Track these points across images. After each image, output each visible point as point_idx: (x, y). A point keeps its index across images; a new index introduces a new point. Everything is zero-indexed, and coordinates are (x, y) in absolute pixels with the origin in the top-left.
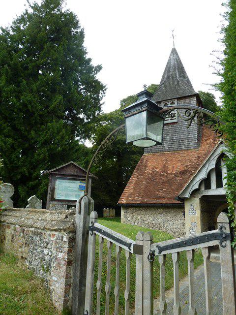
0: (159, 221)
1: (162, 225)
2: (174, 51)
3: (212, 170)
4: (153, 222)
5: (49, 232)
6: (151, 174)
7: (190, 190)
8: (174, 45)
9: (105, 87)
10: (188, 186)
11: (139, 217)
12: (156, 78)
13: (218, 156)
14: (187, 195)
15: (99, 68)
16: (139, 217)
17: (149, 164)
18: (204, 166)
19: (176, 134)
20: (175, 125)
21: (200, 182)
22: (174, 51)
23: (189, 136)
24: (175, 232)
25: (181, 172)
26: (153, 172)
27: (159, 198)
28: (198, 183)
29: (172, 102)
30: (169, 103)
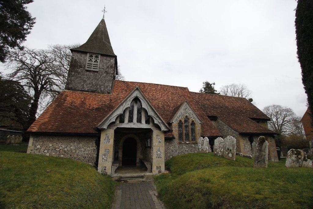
0: (72, 148)
1: (74, 151)
2: (103, 22)
3: (126, 109)
4: (66, 149)
6: (70, 108)
7: (108, 123)
9: (32, 20)
10: (107, 119)
11: (51, 145)
12: (82, 39)
13: (133, 98)
14: (105, 127)
16: (51, 145)
18: (122, 104)
19: (96, 81)
20: (96, 73)
21: (116, 116)
22: (103, 22)
23: (105, 84)
24: (85, 157)
25: (96, 109)
26: (72, 105)
27: (75, 128)
28: (115, 118)
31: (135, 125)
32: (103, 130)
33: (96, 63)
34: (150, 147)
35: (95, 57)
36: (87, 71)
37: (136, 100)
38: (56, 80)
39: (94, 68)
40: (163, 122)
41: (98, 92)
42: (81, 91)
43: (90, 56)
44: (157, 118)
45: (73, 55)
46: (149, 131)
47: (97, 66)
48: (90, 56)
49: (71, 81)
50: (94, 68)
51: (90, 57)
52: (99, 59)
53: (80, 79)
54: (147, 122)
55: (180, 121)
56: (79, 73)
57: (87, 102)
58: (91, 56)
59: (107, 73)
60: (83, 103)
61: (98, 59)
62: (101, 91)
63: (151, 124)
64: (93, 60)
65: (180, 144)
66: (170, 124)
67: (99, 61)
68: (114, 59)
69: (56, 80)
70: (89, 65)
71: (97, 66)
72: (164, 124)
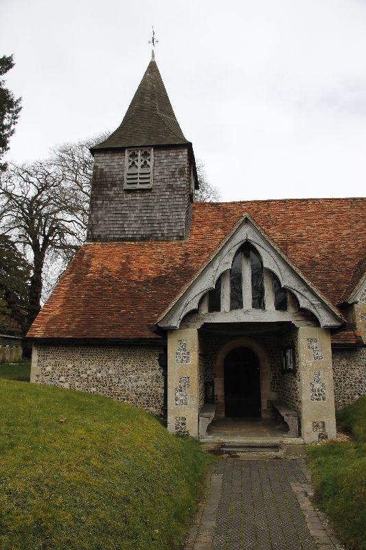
2: (153, 68)
8: (153, 56)
14: (175, 323)
22: (153, 68)
29: (146, 153)
31: (248, 314)
34: (294, 372)
35: (142, 155)
36: (128, 191)
38: (69, 222)
40: (323, 303)
41: (157, 239)
42: (119, 240)
44: (307, 294)
46: (287, 331)
47: (147, 176)
48: (131, 156)
49: (98, 221)
51: (131, 159)
57: (134, 266)
58: (134, 155)
60: (125, 269)
61: (149, 160)
62: (163, 235)
63: (291, 310)
64: (139, 164)
67: (150, 163)
68: (185, 152)
70: (130, 177)
71: (147, 176)
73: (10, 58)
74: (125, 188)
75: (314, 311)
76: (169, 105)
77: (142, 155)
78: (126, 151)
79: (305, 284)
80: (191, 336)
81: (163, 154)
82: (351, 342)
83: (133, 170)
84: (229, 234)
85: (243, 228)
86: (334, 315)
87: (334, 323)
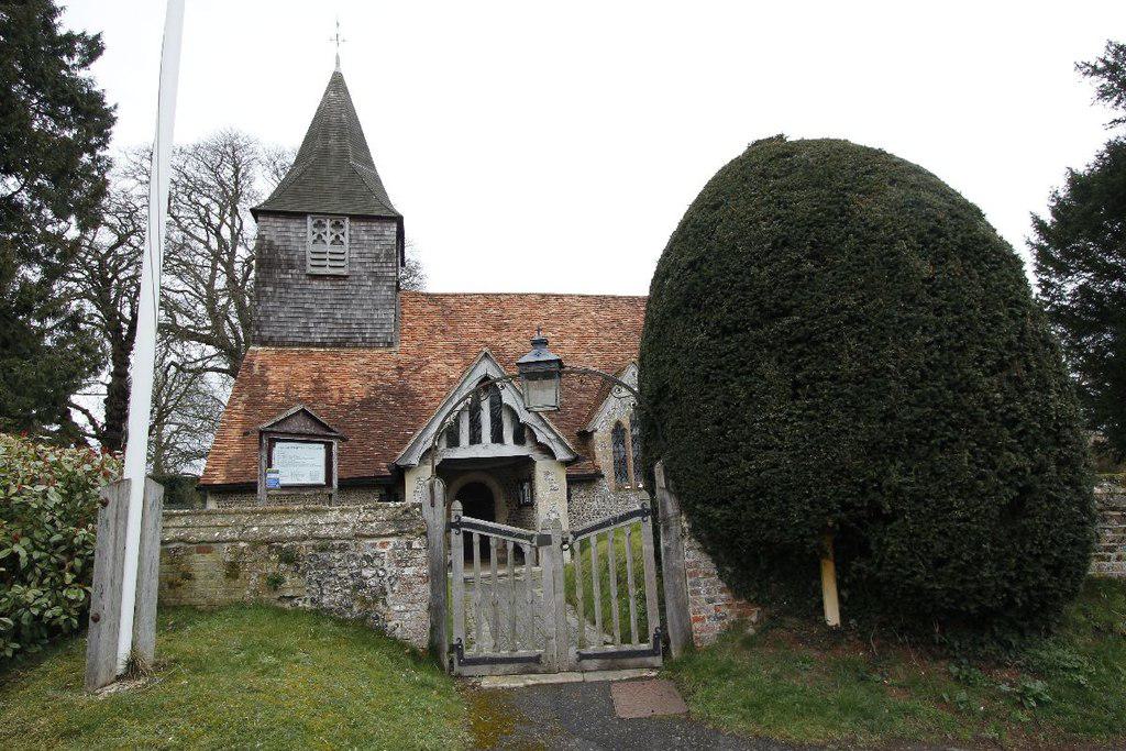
2: (337, 83)
5: (370, 541)
8: (338, 64)
10: (417, 441)
14: (415, 460)
15: (94, 48)
17: (272, 376)
22: (337, 83)
29: (337, 223)
30: (328, 223)
31: (487, 450)
32: (409, 468)
33: (337, 249)
34: (531, 505)
35: (333, 226)
37: (487, 384)
38: (177, 292)
39: (333, 264)
40: (558, 438)
41: (356, 346)
42: (301, 344)
43: (315, 226)
44: (543, 429)
45: (262, 229)
46: (526, 463)
47: (341, 257)
48: (315, 226)
49: (268, 317)
50: (333, 264)
51: (316, 230)
52: (347, 234)
53: (293, 305)
54: (519, 439)
55: (618, 424)
56: (287, 286)
57: (333, 382)
58: (319, 225)
59: (377, 278)
60: (319, 387)
61: (343, 234)
62: (364, 339)
63: (529, 444)
64: (329, 239)
65: (620, 490)
66: (585, 437)
67: (345, 240)
68: (394, 228)
69: (177, 292)
70: (315, 256)
71: (341, 257)
72: (563, 444)
73: (98, 37)
74: (308, 272)
75: (550, 445)
76: (365, 148)
77: (333, 226)
78: (309, 218)
79: (543, 420)
80: (427, 471)
81: (363, 226)
82: (589, 472)
83: (319, 247)
84: (469, 366)
85: (482, 363)
86: (568, 448)
87: (568, 457)
